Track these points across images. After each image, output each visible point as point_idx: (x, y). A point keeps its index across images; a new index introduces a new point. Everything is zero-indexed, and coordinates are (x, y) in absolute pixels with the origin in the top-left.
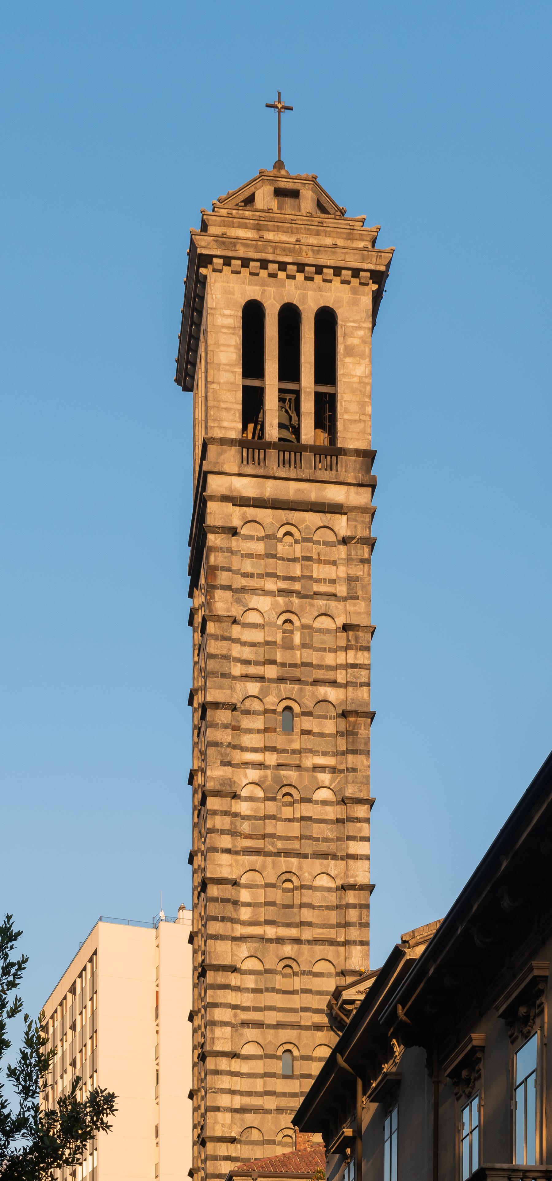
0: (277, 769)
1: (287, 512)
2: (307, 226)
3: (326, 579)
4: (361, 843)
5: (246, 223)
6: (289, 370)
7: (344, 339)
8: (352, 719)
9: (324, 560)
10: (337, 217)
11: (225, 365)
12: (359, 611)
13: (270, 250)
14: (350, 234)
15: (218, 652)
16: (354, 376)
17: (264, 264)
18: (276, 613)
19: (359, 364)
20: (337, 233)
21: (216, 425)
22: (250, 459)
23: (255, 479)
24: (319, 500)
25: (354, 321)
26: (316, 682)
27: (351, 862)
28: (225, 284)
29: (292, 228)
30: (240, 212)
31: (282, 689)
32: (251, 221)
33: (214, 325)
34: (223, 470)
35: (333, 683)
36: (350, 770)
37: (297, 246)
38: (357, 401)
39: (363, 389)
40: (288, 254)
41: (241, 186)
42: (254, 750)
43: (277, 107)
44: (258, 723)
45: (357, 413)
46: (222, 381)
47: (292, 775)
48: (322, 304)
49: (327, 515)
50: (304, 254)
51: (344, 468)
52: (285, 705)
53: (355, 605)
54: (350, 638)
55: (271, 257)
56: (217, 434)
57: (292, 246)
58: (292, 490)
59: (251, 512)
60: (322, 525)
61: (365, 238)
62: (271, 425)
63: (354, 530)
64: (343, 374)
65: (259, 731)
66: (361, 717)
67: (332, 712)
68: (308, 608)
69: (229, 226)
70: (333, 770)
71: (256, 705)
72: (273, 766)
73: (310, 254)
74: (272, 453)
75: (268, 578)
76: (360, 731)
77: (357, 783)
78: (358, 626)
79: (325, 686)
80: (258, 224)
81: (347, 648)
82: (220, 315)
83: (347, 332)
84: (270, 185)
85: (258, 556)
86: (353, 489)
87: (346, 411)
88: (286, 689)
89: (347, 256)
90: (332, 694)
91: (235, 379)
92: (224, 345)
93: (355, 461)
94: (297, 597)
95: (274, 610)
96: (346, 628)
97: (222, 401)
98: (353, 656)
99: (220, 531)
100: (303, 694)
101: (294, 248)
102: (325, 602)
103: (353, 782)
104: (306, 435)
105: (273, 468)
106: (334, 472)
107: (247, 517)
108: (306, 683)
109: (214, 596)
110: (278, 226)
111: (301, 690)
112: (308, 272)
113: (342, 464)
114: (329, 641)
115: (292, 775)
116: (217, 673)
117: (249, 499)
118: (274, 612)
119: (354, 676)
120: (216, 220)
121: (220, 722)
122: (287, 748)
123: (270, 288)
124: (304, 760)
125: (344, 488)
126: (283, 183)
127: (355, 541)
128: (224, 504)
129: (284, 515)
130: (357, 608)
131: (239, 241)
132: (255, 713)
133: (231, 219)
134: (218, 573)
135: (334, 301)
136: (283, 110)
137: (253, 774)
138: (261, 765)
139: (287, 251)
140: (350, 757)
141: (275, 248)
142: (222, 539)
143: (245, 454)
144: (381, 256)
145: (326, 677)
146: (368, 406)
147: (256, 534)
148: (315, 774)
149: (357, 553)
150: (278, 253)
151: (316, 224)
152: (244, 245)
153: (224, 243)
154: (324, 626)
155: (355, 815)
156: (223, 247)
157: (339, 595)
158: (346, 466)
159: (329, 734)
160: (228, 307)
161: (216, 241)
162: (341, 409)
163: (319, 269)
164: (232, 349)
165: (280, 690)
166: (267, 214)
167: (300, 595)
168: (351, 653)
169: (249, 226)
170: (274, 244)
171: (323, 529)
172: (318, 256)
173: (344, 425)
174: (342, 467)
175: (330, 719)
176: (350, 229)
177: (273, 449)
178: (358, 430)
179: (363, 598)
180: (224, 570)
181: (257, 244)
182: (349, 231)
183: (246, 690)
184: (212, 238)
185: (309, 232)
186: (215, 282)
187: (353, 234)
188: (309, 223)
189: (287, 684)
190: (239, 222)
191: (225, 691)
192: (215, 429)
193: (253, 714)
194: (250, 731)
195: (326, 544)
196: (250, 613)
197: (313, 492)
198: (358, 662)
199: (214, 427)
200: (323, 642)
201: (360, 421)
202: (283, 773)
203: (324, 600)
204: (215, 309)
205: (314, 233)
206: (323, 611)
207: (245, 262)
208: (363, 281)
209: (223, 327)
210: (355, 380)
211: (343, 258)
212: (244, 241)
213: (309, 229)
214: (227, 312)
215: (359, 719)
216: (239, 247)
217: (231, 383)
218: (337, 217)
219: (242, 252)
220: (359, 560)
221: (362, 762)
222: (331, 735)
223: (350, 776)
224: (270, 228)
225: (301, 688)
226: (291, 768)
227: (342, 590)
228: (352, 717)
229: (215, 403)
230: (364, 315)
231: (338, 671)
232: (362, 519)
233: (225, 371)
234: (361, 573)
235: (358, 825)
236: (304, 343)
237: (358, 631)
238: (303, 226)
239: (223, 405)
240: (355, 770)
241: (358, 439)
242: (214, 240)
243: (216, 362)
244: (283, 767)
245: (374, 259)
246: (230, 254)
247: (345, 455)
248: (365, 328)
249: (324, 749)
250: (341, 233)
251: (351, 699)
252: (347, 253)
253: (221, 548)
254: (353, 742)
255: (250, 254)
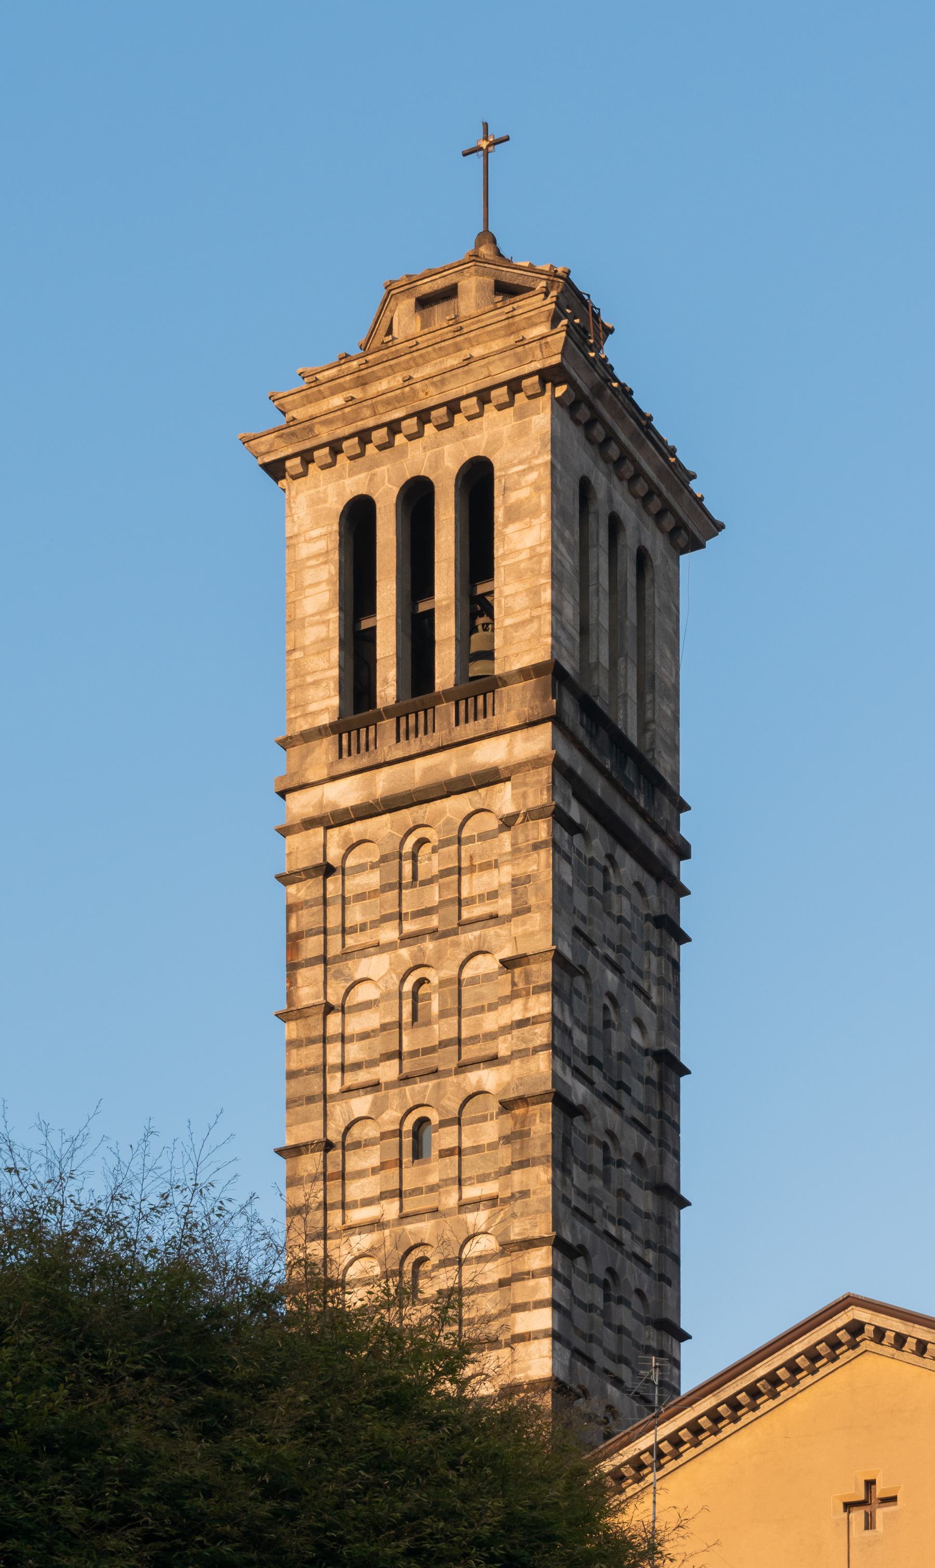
0: (400, 1225)
1: (415, 808)
2: (436, 346)
3: (483, 895)
4: (536, 1311)
5: (340, 384)
6: (417, 579)
7: (504, 498)
8: (519, 1112)
9: (480, 865)
10: (499, 305)
11: (313, 615)
12: (531, 929)
13: (368, 412)
14: (509, 325)
15: (302, 1066)
16: (520, 551)
17: (364, 437)
18: (398, 975)
19: (530, 527)
20: (488, 333)
21: (298, 714)
22: (421, 729)
23: (358, 776)
24: (462, 773)
25: (520, 463)
26: (463, 1067)
27: (519, 1347)
28: (312, 491)
29: (414, 359)
30: (344, 367)
31: (408, 1093)
32: (348, 378)
33: (295, 561)
34: (304, 781)
35: (493, 1060)
36: (517, 1195)
37: (407, 389)
38: (527, 590)
39: (536, 567)
40: (397, 405)
41: (373, 316)
42: (367, 1202)
43: (481, 149)
44: (371, 1157)
45: (526, 609)
46: (307, 643)
47: (424, 1229)
48: (467, 456)
49: (480, 791)
50: (422, 395)
51: (505, 705)
52: (416, 1117)
53: (524, 923)
54: (516, 980)
55: (371, 423)
56: (301, 727)
57: (399, 391)
58: (418, 772)
59: (356, 829)
60: (472, 809)
61: (537, 320)
62: (386, 681)
63: (521, 801)
64: (504, 556)
65: (374, 1171)
66: (533, 1104)
67: (495, 1107)
68: (450, 951)
69: (317, 400)
70: (493, 1201)
71: (369, 1131)
72: (394, 1220)
73: (432, 390)
74: (447, 709)
75: (384, 925)
76: (533, 1128)
77: (529, 1214)
78: (525, 956)
79: (479, 1069)
80: (358, 377)
81: (514, 995)
82: (306, 541)
83: (508, 485)
84: (408, 297)
85: (374, 893)
86: (519, 735)
87: (509, 612)
88: (411, 1093)
89: (491, 368)
90: (490, 1079)
91: (328, 632)
92: (310, 586)
93: (524, 688)
94: (432, 939)
95: (394, 971)
96: (508, 964)
97: (309, 673)
98: (521, 1007)
99: (303, 877)
100: (442, 1092)
101: (403, 393)
102: (477, 933)
103: (522, 1215)
104: (441, 676)
105: (388, 747)
106: (481, 721)
107: (351, 839)
108: (448, 1073)
109: (296, 980)
110: (391, 366)
111: (438, 1087)
112: (436, 419)
113: (501, 700)
114: (490, 992)
115: (424, 1229)
116: (300, 1098)
117: (346, 810)
118: (394, 976)
119: (524, 1040)
120: (294, 401)
121: (305, 1174)
122: (420, 1186)
123: (382, 468)
124: (443, 1199)
125: (504, 740)
126: (427, 285)
127: (520, 819)
128: (311, 831)
129: (408, 816)
130: (526, 927)
131: (315, 421)
132: (369, 1143)
133: (316, 389)
134: (302, 942)
135: (487, 443)
136: (491, 149)
137: (363, 1241)
138: (377, 1224)
139: (392, 404)
140: (517, 1175)
141: (373, 407)
142: (308, 888)
143: (345, 742)
144: (547, 343)
145: (483, 1054)
146: (545, 591)
147: (370, 860)
148: (462, 1216)
149: (527, 836)
150: (381, 411)
151: (450, 335)
152: (324, 423)
153: (293, 434)
154: (481, 971)
155: (526, 1268)
156: (295, 439)
157: (500, 914)
158: (509, 702)
159: (489, 1144)
160: (317, 524)
161: (281, 436)
162: (500, 613)
163: (453, 407)
164: (324, 587)
165: (405, 1095)
166: (386, 352)
167: (437, 934)
168: (518, 1004)
169: (347, 386)
170: (369, 402)
171: (477, 816)
172: (445, 388)
173: (504, 637)
174: (501, 705)
175: (492, 1119)
176: (508, 318)
177: (388, 718)
178: (528, 636)
179: (538, 907)
180: (311, 935)
181: (344, 414)
182: (506, 322)
183: (350, 1111)
184: (273, 435)
185: (443, 353)
186: (297, 493)
187: (514, 324)
188: (439, 340)
189: (415, 1083)
190: (330, 388)
191: (312, 1123)
192: (298, 720)
193: (366, 1145)
194: (360, 1174)
195: (483, 837)
196: (359, 988)
197: (451, 764)
198: (530, 1015)
199: (296, 718)
200: (480, 997)
201: (531, 619)
202: (409, 1227)
203: (476, 930)
204: (297, 535)
205: (451, 350)
206: (474, 949)
207: (335, 447)
208: (530, 393)
209: (309, 558)
210: (525, 555)
211: (486, 373)
212: (323, 418)
213: (440, 349)
214: (315, 533)
215: (531, 1108)
216: (318, 429)
217: (322, 641)
218: (499, 305)
219: (325, 434)
220: (530, 848)
221: (538, 1176)
222: (492, 1146)
223: (518, 1206)
224: (379, 374)
225: (439, 1084)
226: (422, 1217)
227: (504, 905)
228: (519, 1108)
229: (297, 680)
230: (537, 445)
231: (501, 1038)
232: (535, 778)
233: (312, 625)
234: (535, 867)
235: (531, 1283)
236: (438, 531)
237: (528, 963)
238: (430, 349)
239: (309, 679)
240: (525, 1194)
241: (528, 651)
242: (277, 437)
243: (299, 616)
244: (409, 1219)
245: (538, 353)
246: (308, 445)
247: (505, 684)
248: (539, 465)
249: (481, 1172)
250: (494, 331)
251: (518, 1079)
252: (489, 363)
253: (306, 902)
254: (522, 1148)
255: (338, 431)
